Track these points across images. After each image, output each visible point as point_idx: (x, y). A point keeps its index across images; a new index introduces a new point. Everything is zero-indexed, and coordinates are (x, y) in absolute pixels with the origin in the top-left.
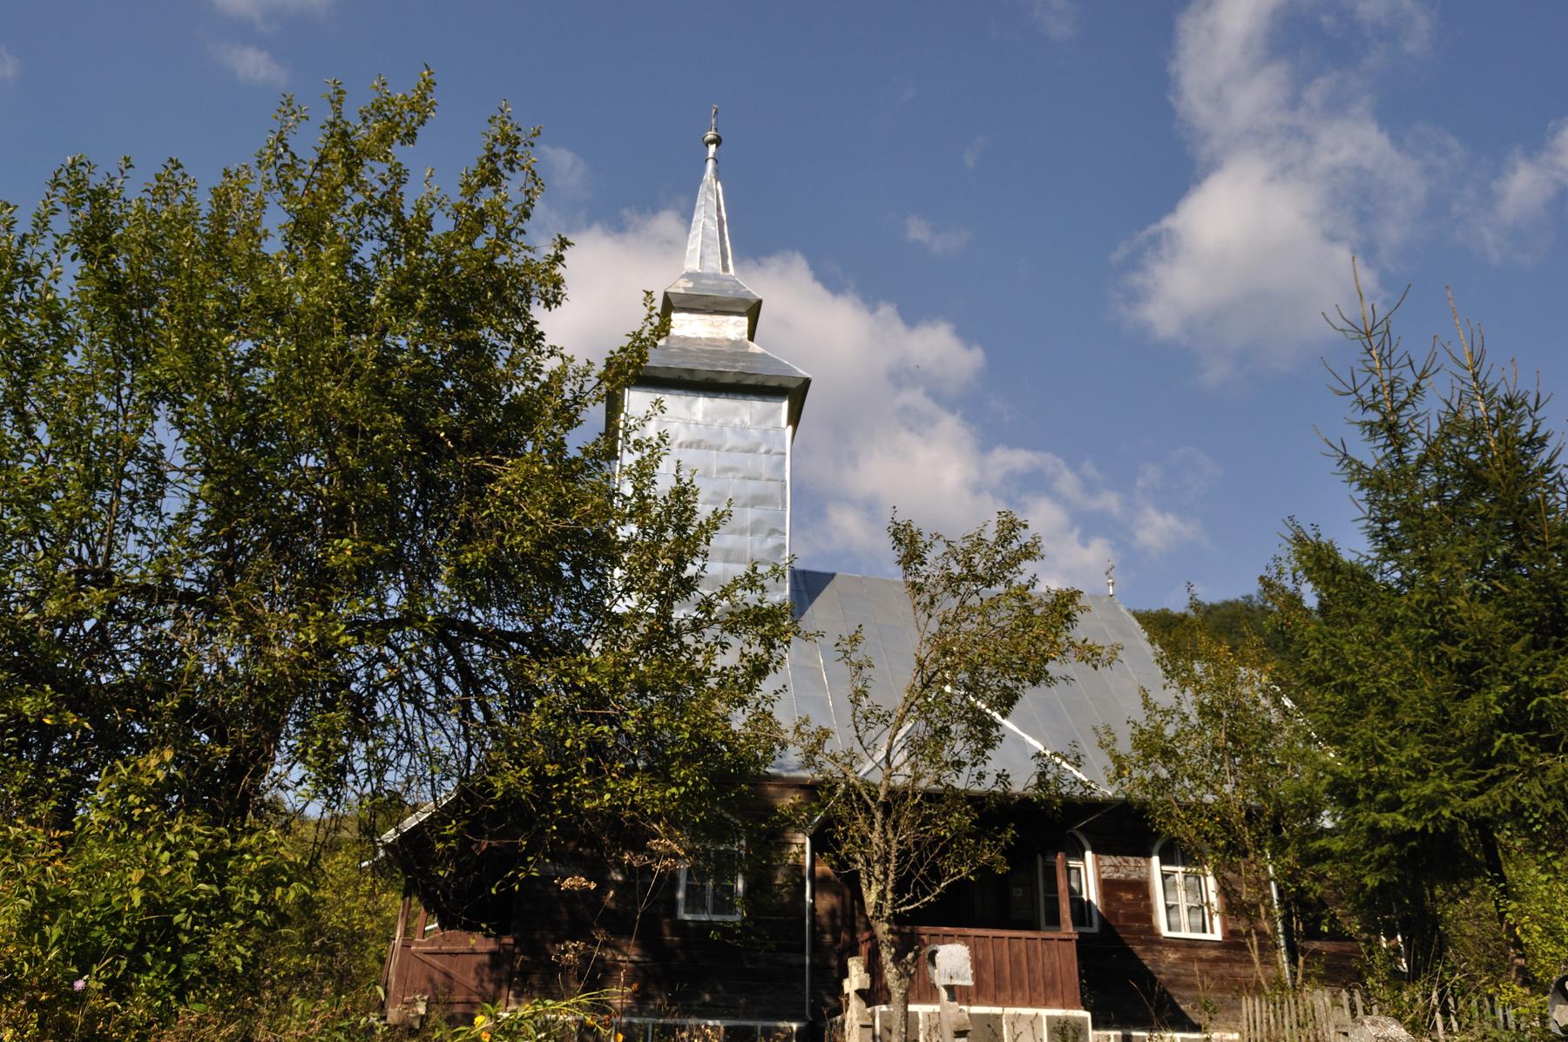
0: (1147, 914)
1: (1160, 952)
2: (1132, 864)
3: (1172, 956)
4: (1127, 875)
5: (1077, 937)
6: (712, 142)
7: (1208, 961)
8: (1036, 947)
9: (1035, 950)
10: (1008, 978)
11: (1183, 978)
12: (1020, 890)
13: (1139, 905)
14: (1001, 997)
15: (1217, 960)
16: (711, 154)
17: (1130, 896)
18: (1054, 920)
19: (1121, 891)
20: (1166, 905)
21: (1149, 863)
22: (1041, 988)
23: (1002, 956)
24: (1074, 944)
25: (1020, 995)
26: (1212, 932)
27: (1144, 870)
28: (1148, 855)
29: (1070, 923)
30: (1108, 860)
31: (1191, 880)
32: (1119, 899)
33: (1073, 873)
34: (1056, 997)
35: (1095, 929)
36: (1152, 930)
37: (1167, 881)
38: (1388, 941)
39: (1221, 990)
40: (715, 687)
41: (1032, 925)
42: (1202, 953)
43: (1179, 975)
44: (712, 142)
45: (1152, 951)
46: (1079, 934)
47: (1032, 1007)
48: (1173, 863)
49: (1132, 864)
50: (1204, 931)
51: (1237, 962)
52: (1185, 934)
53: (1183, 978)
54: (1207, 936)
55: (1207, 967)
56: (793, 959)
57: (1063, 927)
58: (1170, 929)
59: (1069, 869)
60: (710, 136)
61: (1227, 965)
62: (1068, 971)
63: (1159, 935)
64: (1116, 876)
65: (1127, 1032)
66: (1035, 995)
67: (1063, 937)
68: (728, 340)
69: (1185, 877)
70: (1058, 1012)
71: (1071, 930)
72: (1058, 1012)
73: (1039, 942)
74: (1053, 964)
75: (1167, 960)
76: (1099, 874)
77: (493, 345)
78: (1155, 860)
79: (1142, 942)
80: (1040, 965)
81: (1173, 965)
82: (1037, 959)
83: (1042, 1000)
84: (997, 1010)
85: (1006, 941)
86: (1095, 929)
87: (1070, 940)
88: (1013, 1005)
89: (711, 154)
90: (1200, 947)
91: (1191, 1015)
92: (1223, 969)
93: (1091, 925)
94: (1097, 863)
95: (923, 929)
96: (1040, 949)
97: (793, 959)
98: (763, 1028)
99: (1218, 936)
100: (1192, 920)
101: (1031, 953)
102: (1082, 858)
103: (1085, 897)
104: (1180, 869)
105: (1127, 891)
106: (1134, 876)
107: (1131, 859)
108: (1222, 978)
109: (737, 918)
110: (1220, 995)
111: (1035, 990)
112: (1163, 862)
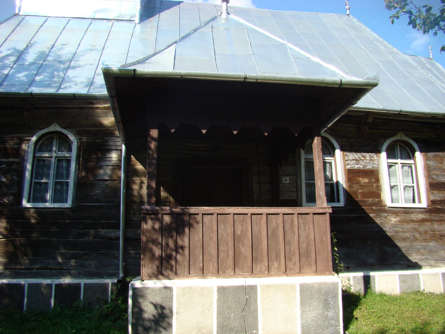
0: (377, 194)
1: (386, 217)
2: (368, 158)
3: (394, 220)
4: (365, 166)
5: (330, 211)
7: (417, 221)
8: (292, 221)
10: (265, 251)
11: (401, 234)
12: (288, 178)
13: (372, 186)
14: (257, 268)
15: (423, 221)
17: (366, 180)
18: (312, 199)
19: (359, 176)
20: (390, 185)
21: (379, 157)
22: (296, 258)
23: (260, 231)
24: (327, 217)
25: (276, 265)
26: (420, 201)
27: (376, 162)
28: (378, 151)
29: (325, 199)
30: (351, 156)
31: (406, 168)
32: (358, 183)
33: (328, 165)
34: (309, 265)
35: (342, 204)
36: (380, 203)
37: (391, 169)
38: (360, 193)
39: (425, 240)
41: (295, 203)
42: (414, 217)
43: (398, 232)
45: (380, 217)
46: (332, 207)
48: (394, 157)
49: (368, 158)
50: (414, 201)
51: (435, 221)
52: (402, 204)
53: (401, 234)
54: (417, 205)
55: (416, 225)
56: (111, 233)
57: (318, 202)
58: (392, 202)
59: (325, 163)
61: (429, 223)
62: (322, 241)
63: (385, 206)
64: (356, 167)
65: (367, 274)
66: (290, 264)
67: (317, 211)
69: (403, 166)
71: (325, 205)
73: (295, 216)
74: (308, 236)
75: (390, 223)
76: (345, 166)
78: (383, 155)
79: (374, 211)
80: (296, 237)
81: (395, 226)
82: (293, 232)
83: (297, 269)
85: (264, 217)
86: (342, 204)
87: (324, 214)
90: (412, 213)
91: (375, 219)
92: (426, 226)
93: (338, 201)
94: (344, 158)
95: (193, 210)
96: (296, 223)
97: (111, 233)
99: (424, 204)
100: (406, 195)
101: (287, 226)
104: (399, 161)
105: (435, 77)
106: (369, 167)
107: (367, 155)
108: (426, 232)
109: (25, 204)
110: (424, 244)
111: (290, 260)
112: (388, 157)
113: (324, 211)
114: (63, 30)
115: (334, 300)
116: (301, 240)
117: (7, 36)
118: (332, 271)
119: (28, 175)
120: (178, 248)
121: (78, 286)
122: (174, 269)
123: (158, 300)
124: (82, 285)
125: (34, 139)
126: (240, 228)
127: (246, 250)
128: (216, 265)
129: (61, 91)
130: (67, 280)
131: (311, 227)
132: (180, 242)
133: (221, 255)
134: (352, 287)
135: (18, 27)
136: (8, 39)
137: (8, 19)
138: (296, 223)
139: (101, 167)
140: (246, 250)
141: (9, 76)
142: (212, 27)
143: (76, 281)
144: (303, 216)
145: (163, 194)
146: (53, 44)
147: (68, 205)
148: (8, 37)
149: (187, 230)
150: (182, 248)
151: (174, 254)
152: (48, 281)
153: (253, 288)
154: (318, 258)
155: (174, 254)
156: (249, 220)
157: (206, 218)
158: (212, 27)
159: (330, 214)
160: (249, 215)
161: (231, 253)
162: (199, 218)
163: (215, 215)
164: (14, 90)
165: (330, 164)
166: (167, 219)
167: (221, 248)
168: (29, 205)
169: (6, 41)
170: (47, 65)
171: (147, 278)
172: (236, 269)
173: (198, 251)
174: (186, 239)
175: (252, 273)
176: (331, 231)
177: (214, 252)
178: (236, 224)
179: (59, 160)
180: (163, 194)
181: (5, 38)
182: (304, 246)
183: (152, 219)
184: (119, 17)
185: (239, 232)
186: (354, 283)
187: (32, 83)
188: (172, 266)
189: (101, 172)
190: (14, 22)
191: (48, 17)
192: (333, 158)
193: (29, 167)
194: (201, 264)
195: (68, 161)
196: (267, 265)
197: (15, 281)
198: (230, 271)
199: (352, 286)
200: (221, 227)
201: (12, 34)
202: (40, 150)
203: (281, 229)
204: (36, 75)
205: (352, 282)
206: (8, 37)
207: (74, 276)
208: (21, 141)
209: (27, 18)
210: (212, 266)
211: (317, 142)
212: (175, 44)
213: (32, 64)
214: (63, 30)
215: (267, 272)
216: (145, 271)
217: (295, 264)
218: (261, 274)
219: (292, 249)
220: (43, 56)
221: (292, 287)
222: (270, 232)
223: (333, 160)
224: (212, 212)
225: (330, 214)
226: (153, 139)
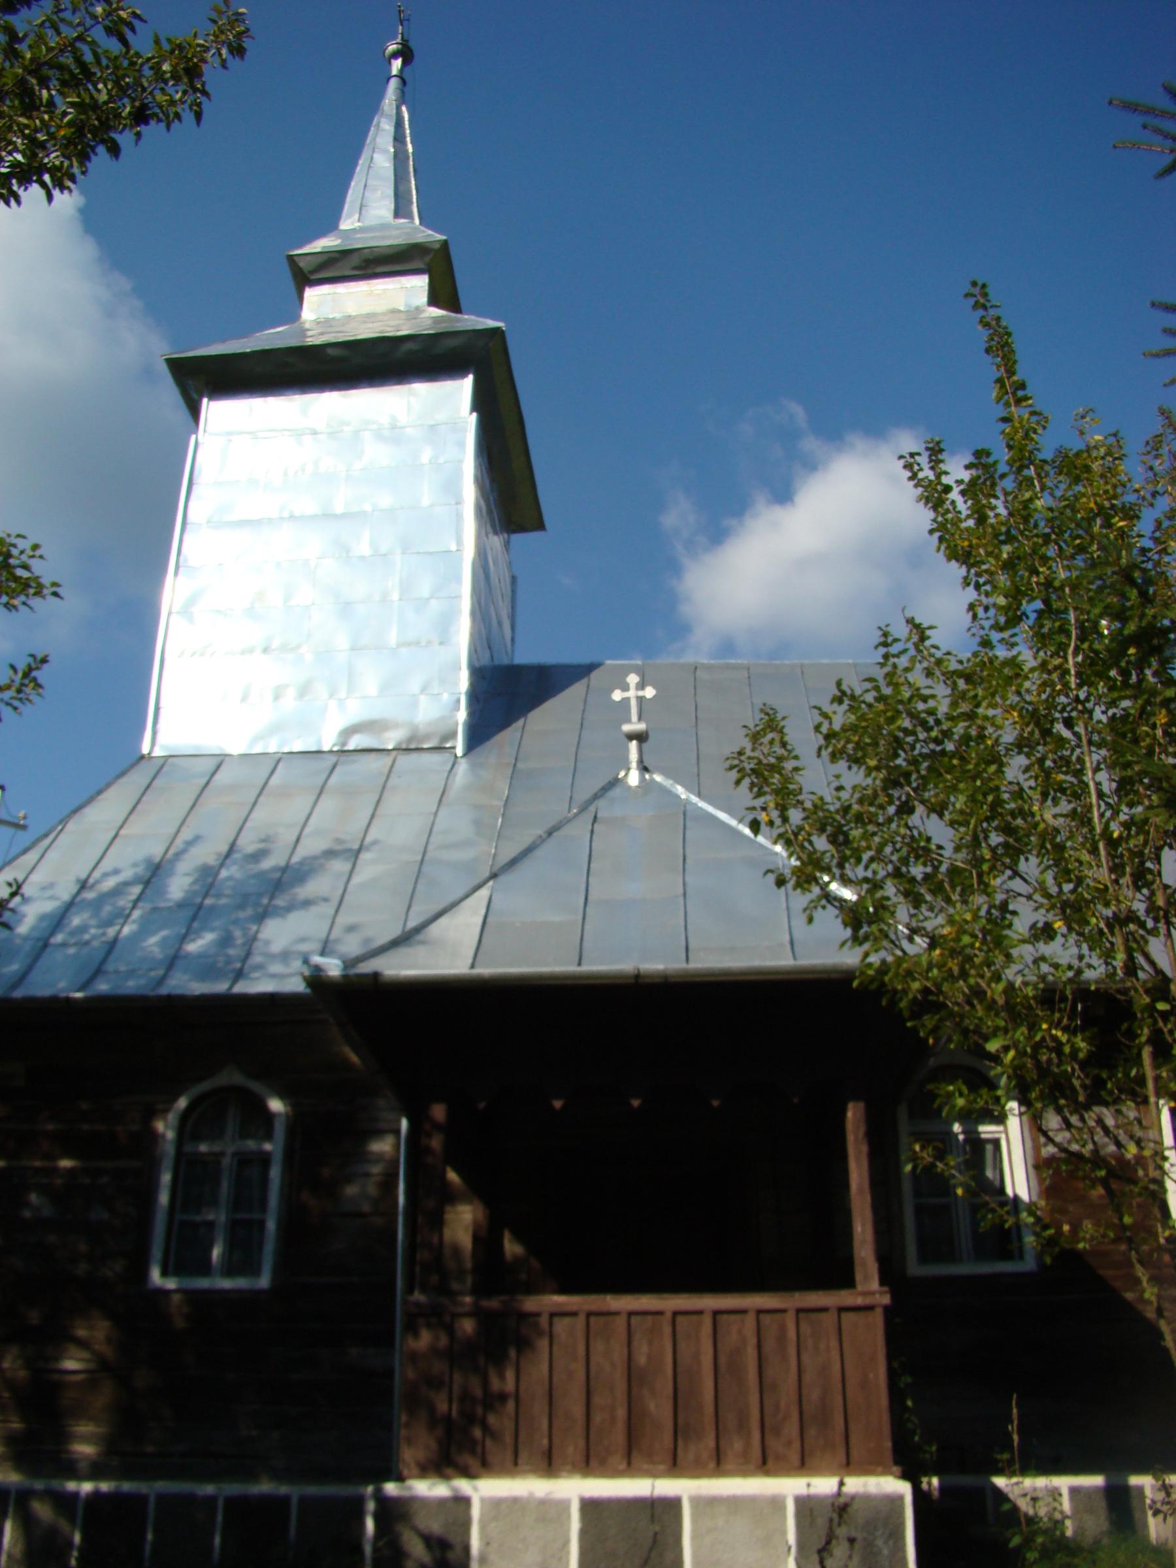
6: (395, 55)
8: (783, 1329)
9: (782, 1338)
10: (709, 1409)
14: (688, 1454)
16: (395, 72)
22: (792, 1428)
24: (878, 1317)
25: (738, 1445)
40: (919, 877)
44: (395, 55)
47: (768, 1473)
60: (392, 48)
66: (773, 1443)
68: (395, 311)
70: (824, 1485)
72: (824, 1485)
77: (1024, 614)
83: (795, 1457)
84: (666, 1487)
85: (707, 1321)
87: (870, 1308)
88: (718, 1465)
89: (395, 72)
95: (531, 1303)
98: (303, 1500)
101: (770, 1344)
102: (1001, 1119)
103: (1009, 1191)
113: (868, 1301)
114: (259, 795)
115: (891, 1542)
116: (807, 1378)
117: (119, 823)
118: (891, 1463)
119: (164, 1198)
120: (494, 1400)
121: (285, 1500)
122: (479, 1449)
123: (435, 1526)
124: (294, 1501)
125: (182, 1103)
126: (645, 1348)
127: (658, 1407)
128: (582, 1443)
129: (241, 988)
130: (264, 1487)
131: (834, 1343)
132: (495, 1384)
133: (597, 1418)
134: (1068, 1523)
135: (149, 792)
136: (122, 832)
137: (123, 774)
138: (792, 1334)
139: (349, 1180)
140: (658, 1407)
141: (119, 946)
142: (595, 817)
143: (284, 1489)
144: (814, 1316)
145: (511, 1247)
146: (231, 840)
147: (264, 1281)
148: (121, 827)
149: (513, 1353)
150: (503, 1397)
151: (479, 1410)
152: (209, 1489)
153: (672, 1506)
154: (853, 1427)
155: (479, 1410)
156: (667, 1330)
157: (561, 1325)
158: (595, 817)
159: (886, 1309)
160: (669, 1315)
161: (621, 1413)
162: (544, 1321)
163: (581, 1319)
164: (132, 986)
165: (996, 1143)
166: (468, 1326)
167: (597, 1400)
168: (171, 1284)
169: (117, 841)
170: (212, 908)
171: (415, 1471)
172: (635, 1453)
173: (539, 1409)
174: (510, 1375)
175: (675, 1466)
176: (890, 1357)
177: (578, 1411)
178: (637, 1337)
179: (244, 1160)
180: (511, 1247)
181: (113, 833)
182: (813, 1395)
183: (429, 1326)
184: (411, 739)
185: (641, 1360)
186: (1075, 1509)
187: (173, 961)
188: (474, 1442)
189: (351, 1190)
190: (137, 779)
191: (222, 757)
192: (1001, 1128)
193: (166, 1178)
194: (545, 1442)
195: (265, 1160)
196: (711, 1443)
197: (127, 1486)
198: (618, 1461)
199: (1068, 1517)
200: (598, 1346)
201: (132, 818)
202: (197, 1137)
203: (751, 1353)
204: (183, 939)
205: (1066, 1505)
206: (121, 827)
207: (277, 1476)
208: (151, 1113)
209: (170, 760)
210: (572, 1448)
211: (854, 1114)
212: (491, 883)
213: (181, 905)
214: (259, 795)
215: (712, 1465)
216: (409, 1455)
217: (789, 1443)
218: (697, 1470)
219: (783, 1404)
220: (208, 877)
221: (776, 1503)
222: (723, 1359)
223: (1000, 1132)
224: (574, 1308)
225: (886, 1309)
226: (437, 1126)
